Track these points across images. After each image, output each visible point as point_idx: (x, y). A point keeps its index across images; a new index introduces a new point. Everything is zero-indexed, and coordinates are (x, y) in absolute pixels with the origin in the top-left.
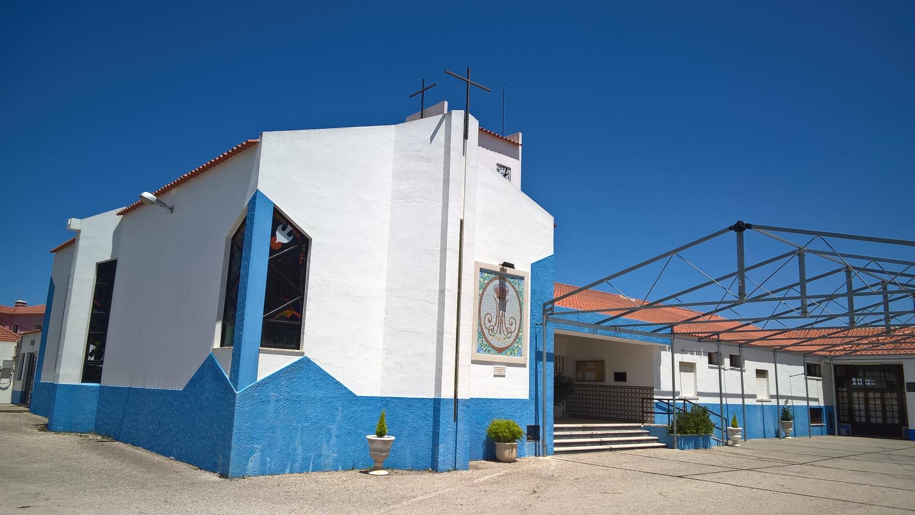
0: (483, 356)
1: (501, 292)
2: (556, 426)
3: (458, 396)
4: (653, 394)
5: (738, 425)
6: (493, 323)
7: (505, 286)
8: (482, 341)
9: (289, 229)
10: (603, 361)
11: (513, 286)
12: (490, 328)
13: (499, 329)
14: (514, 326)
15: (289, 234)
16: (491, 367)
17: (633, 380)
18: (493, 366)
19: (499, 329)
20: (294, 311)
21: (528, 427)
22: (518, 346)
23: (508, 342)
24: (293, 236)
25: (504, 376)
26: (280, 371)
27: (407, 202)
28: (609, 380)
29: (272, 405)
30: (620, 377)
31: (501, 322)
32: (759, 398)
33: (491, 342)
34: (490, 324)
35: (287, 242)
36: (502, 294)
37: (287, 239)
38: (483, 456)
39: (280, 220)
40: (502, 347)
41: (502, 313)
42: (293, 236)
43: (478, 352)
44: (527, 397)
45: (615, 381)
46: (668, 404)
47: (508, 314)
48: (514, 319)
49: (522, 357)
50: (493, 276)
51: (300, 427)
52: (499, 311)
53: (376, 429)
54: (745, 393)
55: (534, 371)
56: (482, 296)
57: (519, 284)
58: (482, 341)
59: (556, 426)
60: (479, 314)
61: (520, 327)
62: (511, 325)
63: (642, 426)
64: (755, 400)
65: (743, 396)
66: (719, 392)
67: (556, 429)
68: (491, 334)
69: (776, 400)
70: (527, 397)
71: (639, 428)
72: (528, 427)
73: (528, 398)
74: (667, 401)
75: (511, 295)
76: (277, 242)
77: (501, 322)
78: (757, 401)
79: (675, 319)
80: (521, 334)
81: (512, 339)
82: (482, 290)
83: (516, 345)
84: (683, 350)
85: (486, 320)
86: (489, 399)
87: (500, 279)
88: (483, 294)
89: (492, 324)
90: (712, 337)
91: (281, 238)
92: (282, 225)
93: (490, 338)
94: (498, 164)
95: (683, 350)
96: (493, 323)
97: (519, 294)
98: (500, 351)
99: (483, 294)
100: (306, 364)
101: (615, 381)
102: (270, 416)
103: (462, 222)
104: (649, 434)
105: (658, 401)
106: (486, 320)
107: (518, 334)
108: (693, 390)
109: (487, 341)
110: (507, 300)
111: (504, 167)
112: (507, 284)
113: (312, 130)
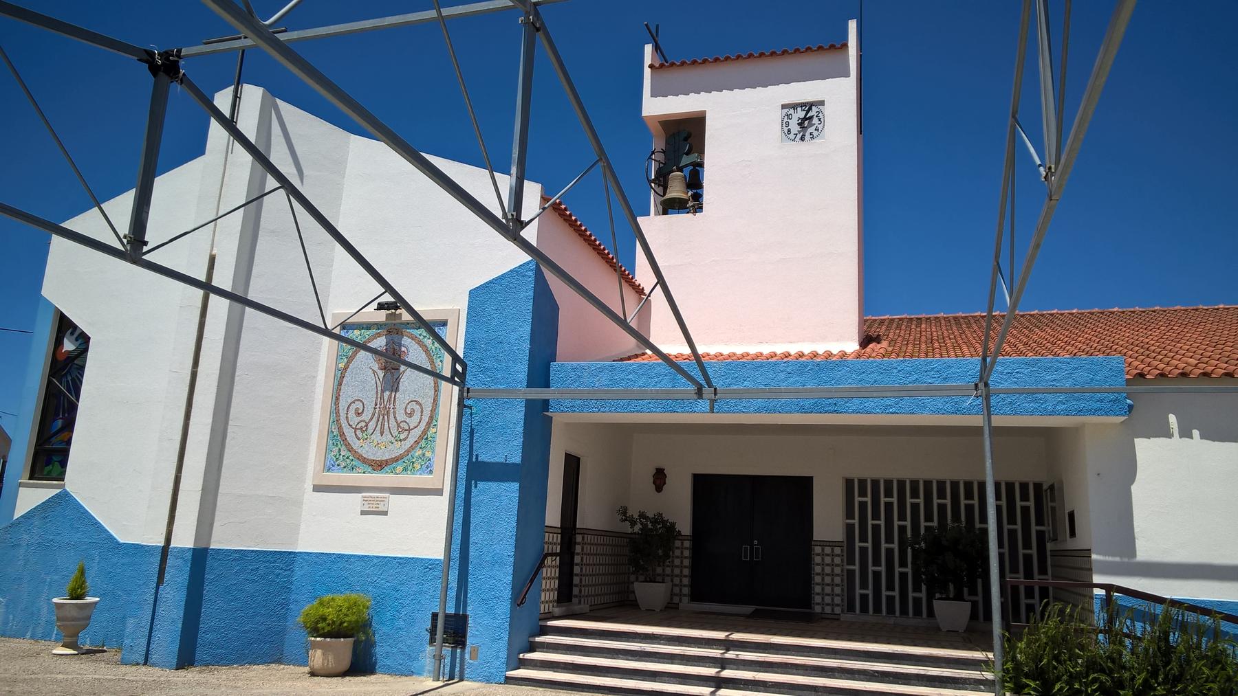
7: (400, 345)
8: (340, 449)
12: (359, 426)
13: (379, 426)
18: (360, 495)
19: (379, 426)
22: (424, 455)
23: (397, 449)
25: (385, 513)
31: (384, 411)
33: (359, 451)
34: (359, 419)
39: (64, 325)
40: (384, 458)
41: (390, 397)
43: (328, 471)
48: (417, 402)
52: (383, 391)
61: (431, 418)
62: (410, 415)
68: (360, 436)
77: (384, 411)
80: (434, 430)
82: (346, 360)
85: (352, 414)
87: (389, 332)
89: (363, 417)
93: (356, 444)
94: (784, 107)
96: (366, 416)
98: (379, 466)
100: (64, 498)
106: (352, 414)
107: (425, 432)
109: (350, 449)
111: (802, 105)
112: (406, 341)
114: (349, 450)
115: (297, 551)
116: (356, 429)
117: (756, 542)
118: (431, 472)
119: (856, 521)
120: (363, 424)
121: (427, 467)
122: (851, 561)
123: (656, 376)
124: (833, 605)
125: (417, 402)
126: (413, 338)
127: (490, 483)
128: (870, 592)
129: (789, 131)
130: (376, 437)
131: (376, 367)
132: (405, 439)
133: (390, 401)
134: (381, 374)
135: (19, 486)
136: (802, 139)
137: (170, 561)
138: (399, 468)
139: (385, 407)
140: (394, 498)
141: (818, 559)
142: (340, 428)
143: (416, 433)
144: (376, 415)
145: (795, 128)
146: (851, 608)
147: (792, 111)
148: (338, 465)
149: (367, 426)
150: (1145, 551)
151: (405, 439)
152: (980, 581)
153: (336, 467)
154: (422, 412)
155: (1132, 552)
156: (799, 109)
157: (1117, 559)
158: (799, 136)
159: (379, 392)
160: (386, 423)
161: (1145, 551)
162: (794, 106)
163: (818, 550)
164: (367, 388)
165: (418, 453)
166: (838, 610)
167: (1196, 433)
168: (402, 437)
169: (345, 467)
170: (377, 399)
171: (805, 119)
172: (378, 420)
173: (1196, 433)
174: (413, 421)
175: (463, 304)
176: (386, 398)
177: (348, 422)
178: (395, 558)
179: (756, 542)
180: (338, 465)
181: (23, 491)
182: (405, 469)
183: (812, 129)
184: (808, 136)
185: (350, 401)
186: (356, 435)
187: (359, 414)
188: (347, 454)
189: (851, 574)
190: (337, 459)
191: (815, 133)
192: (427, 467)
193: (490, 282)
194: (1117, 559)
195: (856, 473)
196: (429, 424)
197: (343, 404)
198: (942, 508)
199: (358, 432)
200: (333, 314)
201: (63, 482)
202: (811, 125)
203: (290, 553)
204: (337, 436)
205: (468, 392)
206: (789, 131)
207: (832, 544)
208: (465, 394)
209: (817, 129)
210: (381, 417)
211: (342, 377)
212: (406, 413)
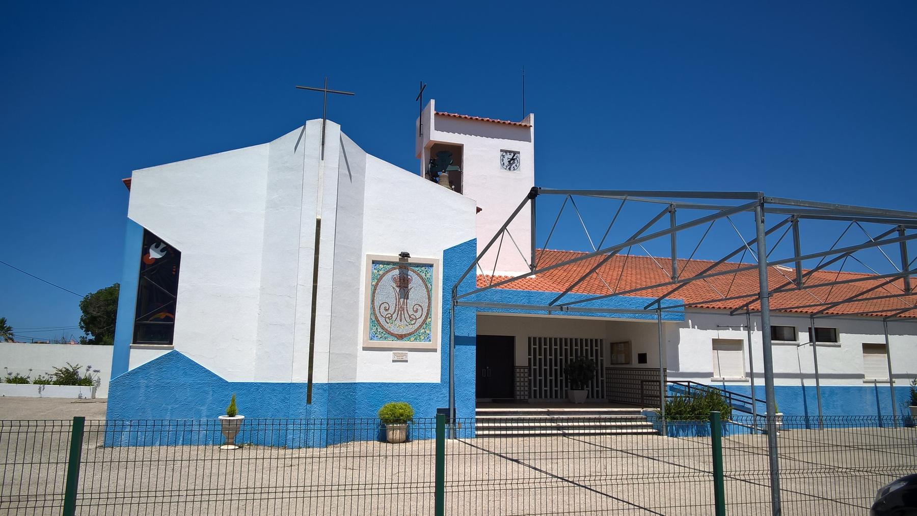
0: (376, 343)
1: (402, 281)
2: (477, 410)
3: (313, 381)
4: (666, 376)
5: (777, 411)
6: (391, 311)
7: (407, 275)
8: (377, 329)
9: (162, 246)
10: (627, 342)
11: (418, 274)
12: (387, 316)
13: (399, 316)
14: (419, 313)
15: (162, 251)
16: (390, 354)
17: (651, 363)
18: (392, 352)
19: (399, 316)
20: (169, 313)
21: (439, 411)
22: (425, 332)
23: (411, 329)
24: (166, 252)
25: (407, 361)
26: (150, 363)
27: (277, 210)
28: (635, 363)
29: (142, 390)
30: (643, 358)
31: (401, 309)
32: (867, 378)
33: (388, 329)
34: (387, 312)
35: (161, 257)
36: (403, 284)
37: (161, 255)
38: (378, 437)
39: (150, 239)
40: (404, 333)
41: (404, 302)
42: (166, 252)
43: (371, 339)
44: (439, 381)
45: (639, 363)
46: (689, 386)
47: (411, 302)
48: (420, 305)
49: (431, 343)
50: (391, 266)
51: (170, 408)
52: (399, 299)
53: (227, 409)
54: (754, 371)
55: (447, 355)
56: (375, 288)
57: (427, 271)
58: (377, 329)
59: (477, 410)
60: (373, 301)
61: (428, 314)
62: (416, 311)
63: (642, 411)
64: (709, 379)
65: (817, 376)
66: (814, 372)
67: (478, 413)
68: (388, 321)
69: (815, 380)
70: (439, 381)
71: (639, 412)
72: (439, 411)
73: (440, 382)
74: (687, 384)
75: (415, 281)
76: (150, 258)
77: (401, 309)
78: (864, 382)
79: (839, 288)
80: (430, 320)
81: (417, 325)
82: (376, 281)
83: (422, 331)
84: (718, 326)
85: (382, 310)
86: (386, 383)
87: (400, 268)
88: (377, 284)
89: (389, 312)
90: (826, 312)
91: (154, 254)
92: (155, 244)
93: (386, 326)
94: (501, 151)
95: (718, 326)
96: (391, 311)
97: (427, 284)
98: (401, 337)
99: (377, 284)
100: (175, 356)
101: (639, 363)
102: (140, 399)
103: (319, 222)
104: (646, 420)
105: (673, 384)
106: (382, 310)
107: (425, 321)
108: (742, 371)
109: (382, 328)
110: (409, 288)
111: (510, 152)
112: (410, 273)
113: (180, 162)
114: (382, 329)
115: (357, 382)
116: (385, 318)
117: (488, 368)
118: (430, 341)
119: (532, 357)
120: (390, 315)
121: (428, 338)
122: (530, 375)
123: (522, 296)
124: (524, 395)
125: (420, 305)
126: (414, 272)
127: (462, 346)
128: (538, 389)
129: (504, 163)
130: (398, 322)
131: (394, 286)
132: (414, 324)
133: (404, 304)
134: (398, 290)
135: (130, 348)
136: (510, 169)
137: (314, 390)
138: (412, 339)
139: (401, 307)
140: (410, 354)
141: (518, 375)
142: (376, 318)
143: (420, 321)
144: (397, 311)
145: (506, 163)
146: (530, 397)
147: (504, 154)
148: (377, 337)
149: (392, 316)
150: (682, 369)
151: (414, 324)
152: (590, 382)
153: (375, 338)
154: (422, 310)
155: (678, 369)
156: (508, 153)
157: (674, 372)
158: (508, 167)
159: (398, 299)
160: (403, 315)
161: (682, 369)
162: (506, 152)
163: (518, 370)
164: (390, 296)
165: (422, 331)
166: (526, 397)
167: (696, 327)
168: (413, 322)
169: (381, 338)
170: (396, 302)
171: (513, 159)
172: (398, 314)
173: (696, 327)
174: (418, 315)
175: (440, 257)
176: (402, 302)
177: (380, 313)
178: (414, 384)
179: (488, 368)
180: (377, 337)
181: (133, 352)
182: (416, 339)
183: (514, 165)
184: (512, 168)
185: (381, 303)
186: (386, 321)
187: (386, 310)
188: (382, 331)
189: (530, 380)
190: (376, 334)
191: (516, 168)
192: (428, 338)
193: (454, 247)
194: (674, 372)
195: (532, 335)
196: (426, 318)
197: (377, 304)
198: (576, 350)
199: (387, 319)
200: (367, 255)
201: (171, 346)
202: (514, 163)
203: (355, 383)
204: (376, 323)
205: (457, 303)
206: (504, 163)
207: (524, 368)
208: (456, 304)
209: (516, 166)
210: (400, 312)
211: (375, 289)
212: (414, 311)
